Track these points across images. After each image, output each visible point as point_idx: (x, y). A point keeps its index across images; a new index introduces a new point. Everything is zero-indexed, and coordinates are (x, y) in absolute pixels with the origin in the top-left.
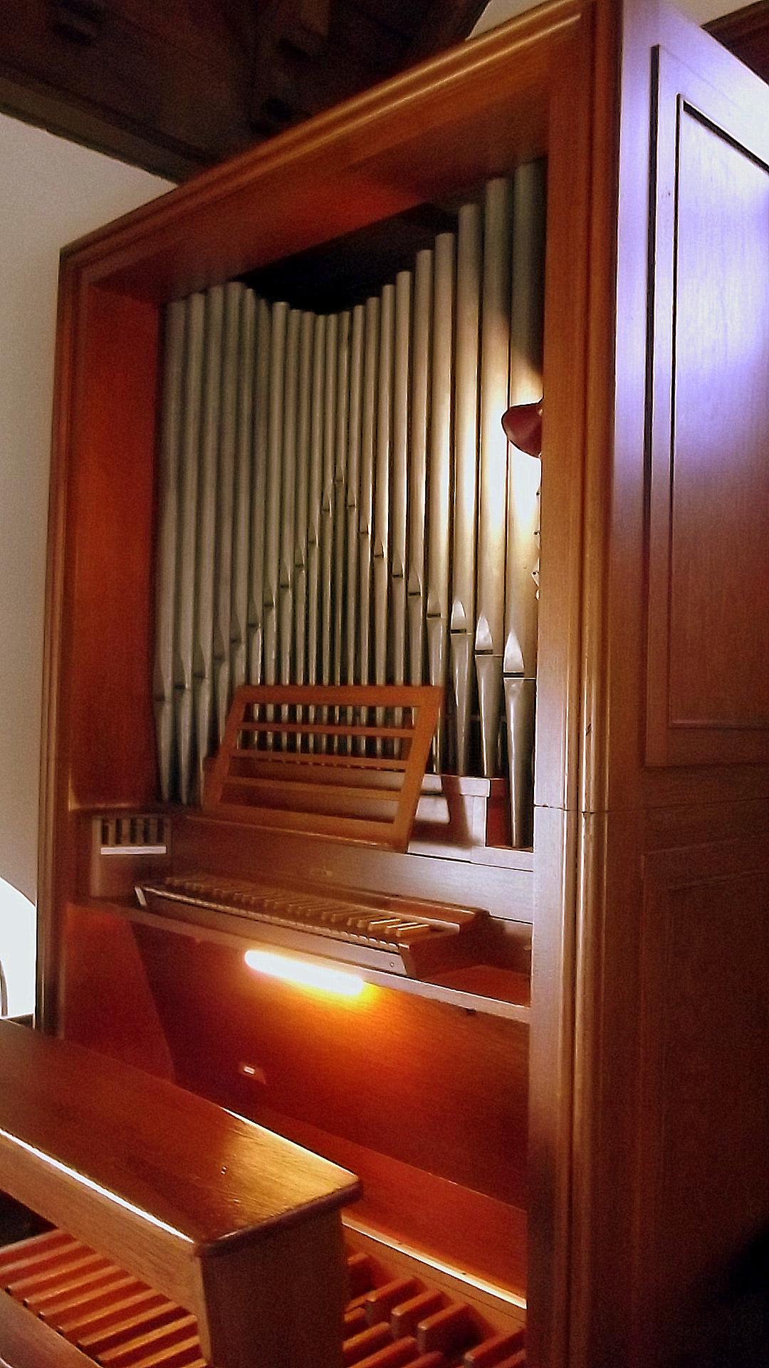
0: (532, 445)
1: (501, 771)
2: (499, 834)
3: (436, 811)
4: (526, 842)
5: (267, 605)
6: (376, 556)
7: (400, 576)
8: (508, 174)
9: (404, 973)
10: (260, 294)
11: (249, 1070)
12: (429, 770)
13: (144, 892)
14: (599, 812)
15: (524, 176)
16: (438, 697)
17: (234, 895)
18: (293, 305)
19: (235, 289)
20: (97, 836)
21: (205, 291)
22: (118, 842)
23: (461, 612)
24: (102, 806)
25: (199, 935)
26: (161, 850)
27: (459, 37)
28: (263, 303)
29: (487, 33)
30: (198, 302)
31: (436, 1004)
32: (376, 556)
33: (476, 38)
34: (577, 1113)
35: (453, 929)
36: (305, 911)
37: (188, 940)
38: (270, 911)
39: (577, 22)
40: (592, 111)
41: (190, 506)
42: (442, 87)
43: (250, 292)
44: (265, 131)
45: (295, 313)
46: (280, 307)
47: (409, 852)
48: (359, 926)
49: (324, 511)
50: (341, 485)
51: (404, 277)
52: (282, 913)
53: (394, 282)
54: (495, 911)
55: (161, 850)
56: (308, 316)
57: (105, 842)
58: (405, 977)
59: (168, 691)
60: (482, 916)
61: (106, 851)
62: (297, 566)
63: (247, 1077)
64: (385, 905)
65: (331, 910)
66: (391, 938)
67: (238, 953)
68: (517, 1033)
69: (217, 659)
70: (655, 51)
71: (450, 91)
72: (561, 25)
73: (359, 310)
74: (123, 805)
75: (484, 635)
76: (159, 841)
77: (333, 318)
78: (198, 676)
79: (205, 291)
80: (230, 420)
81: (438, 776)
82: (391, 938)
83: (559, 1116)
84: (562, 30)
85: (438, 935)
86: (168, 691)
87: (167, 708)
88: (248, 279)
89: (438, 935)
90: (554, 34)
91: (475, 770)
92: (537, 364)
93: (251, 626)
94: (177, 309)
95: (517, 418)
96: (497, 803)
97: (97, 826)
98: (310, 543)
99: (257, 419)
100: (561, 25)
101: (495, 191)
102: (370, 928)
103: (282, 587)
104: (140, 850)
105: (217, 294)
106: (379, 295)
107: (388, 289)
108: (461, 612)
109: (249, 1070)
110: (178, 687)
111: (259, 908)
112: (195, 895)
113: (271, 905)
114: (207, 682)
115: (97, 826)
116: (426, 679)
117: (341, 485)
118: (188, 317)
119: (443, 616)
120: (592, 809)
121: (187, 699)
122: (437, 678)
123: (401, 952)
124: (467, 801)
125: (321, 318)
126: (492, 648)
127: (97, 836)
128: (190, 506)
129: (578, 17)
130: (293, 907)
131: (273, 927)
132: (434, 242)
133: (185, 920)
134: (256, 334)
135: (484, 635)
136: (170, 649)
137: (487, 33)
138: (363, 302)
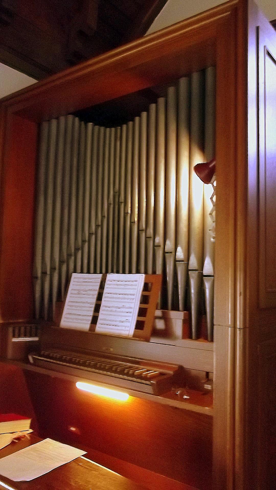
0: (207, 180)
1: (187, 308)
2: (187, 334)
3: (160, 325)
4: (212, 341)
5: (84, 241)
6: (132, 223)
7: (93, 234)
8: (189, 75)
9: (152, 393)
10: (81, 120)
11: (73, 429)
12: (157, 309)
13: (33, 358)
14: (245, 328)
15: (195, 77)
16: (160, 279)
17: (63, 357)
18: (95, 124)
19: (70, 117)
20: (11, 334)
21: (57, 118)
22: (19, 336)
23: (170, 245)
24: (12, 321)
25: (53, 374)
26: (36, 339)
27: (142, 34)
28: (83, 123)
29: (150, 35)
30: (54, 122)
31: (166, 407)
32: (132, 223)
33: (147, 36)
34: (237, 454)
35: (169, 374)
36: (76, 360)
37: (48, 376)
38: (89, 366)
39: (229, 15)
40: (236, 48)
41: (50, 201)
42: (169, 39)
43: (77, 119)
44: (72, 64)
45: (97, 127)
46: (90, 125)
47: (151, 342)
48: (130, 373)
49: (109, 205)
50: (117, 194)
51: (144, 114)
52: (95, 367)
53: (140, 116)
54: (186, 366)
55: (36, 339)
56: (102, 129)
57: (14, 336)
58: (152, 394)
59: (39, 274)
60: (181, 368)
61: (15, 340)
62: (97, 226)
63: (72, 432)
64: (138, 363)
65: (76, 357)
66: (146, 378)
67: (74, 383)
68: (209, 419)
69: (61, 262)
70: (258, 28)
71: (169, 42)
72: (222, 16)
73: (124, 127)
74: (21, 321)
75: (180, 254)
76: (36, 336)
77: (113, 129)
78: (53, 269)
79: (57, 118)
80: (68, 168)
81: (160, 310)
82: (146, 378)
83: (228, 457)
84: (222, 17)
85: (165, 377)
86: (39, 274)
87: (39, 282)
88: (76, 114)
89: (165, 377)
90: (219, 19)
91: (175, 308)
92: (202, 148)
93: (77, 249)
94: (45, 125)
95: (199, 169)
96: (187, 322)
97: (11, 330)
98: (103, 217)
99: (81, 167)
100: (222, 16)
101: (183, 82)
102: (135, 374)
103: (90, 234)
104: (28, 339)
105: (62, 119)
106: (133, 120)
107: (137, 119)
108: (170, 245)
109: (73, 429)
110: (44, 273)
111: (84, 364)
112: (55, 359)
113: (79, 362)
114: (57, 271)
115: (11, 330)
116: (154, 272)
117: (117, 194)
118: (50, 127)
119: (162, 246)
120: (242, 327)
121: (48, 278)
122: (159, 271)
123: (152, 385)
124: (173, 321)
125: (108, 129)
126: (184, 259)
127: (11, 334)
128: (50, 201)
129: (229, 13)
130: (132, 371)
131: (91, 373)
132: (157, 101)
133: (54, 370)
134: (80, 133)
135: (180, 254)
136: (40, 258)
137: (150, 35)
138: (126, 123)
